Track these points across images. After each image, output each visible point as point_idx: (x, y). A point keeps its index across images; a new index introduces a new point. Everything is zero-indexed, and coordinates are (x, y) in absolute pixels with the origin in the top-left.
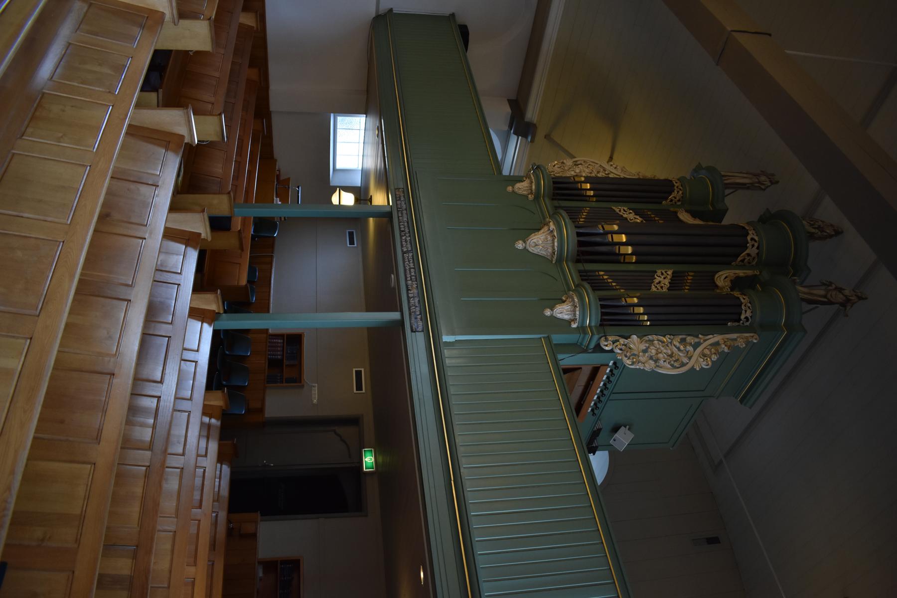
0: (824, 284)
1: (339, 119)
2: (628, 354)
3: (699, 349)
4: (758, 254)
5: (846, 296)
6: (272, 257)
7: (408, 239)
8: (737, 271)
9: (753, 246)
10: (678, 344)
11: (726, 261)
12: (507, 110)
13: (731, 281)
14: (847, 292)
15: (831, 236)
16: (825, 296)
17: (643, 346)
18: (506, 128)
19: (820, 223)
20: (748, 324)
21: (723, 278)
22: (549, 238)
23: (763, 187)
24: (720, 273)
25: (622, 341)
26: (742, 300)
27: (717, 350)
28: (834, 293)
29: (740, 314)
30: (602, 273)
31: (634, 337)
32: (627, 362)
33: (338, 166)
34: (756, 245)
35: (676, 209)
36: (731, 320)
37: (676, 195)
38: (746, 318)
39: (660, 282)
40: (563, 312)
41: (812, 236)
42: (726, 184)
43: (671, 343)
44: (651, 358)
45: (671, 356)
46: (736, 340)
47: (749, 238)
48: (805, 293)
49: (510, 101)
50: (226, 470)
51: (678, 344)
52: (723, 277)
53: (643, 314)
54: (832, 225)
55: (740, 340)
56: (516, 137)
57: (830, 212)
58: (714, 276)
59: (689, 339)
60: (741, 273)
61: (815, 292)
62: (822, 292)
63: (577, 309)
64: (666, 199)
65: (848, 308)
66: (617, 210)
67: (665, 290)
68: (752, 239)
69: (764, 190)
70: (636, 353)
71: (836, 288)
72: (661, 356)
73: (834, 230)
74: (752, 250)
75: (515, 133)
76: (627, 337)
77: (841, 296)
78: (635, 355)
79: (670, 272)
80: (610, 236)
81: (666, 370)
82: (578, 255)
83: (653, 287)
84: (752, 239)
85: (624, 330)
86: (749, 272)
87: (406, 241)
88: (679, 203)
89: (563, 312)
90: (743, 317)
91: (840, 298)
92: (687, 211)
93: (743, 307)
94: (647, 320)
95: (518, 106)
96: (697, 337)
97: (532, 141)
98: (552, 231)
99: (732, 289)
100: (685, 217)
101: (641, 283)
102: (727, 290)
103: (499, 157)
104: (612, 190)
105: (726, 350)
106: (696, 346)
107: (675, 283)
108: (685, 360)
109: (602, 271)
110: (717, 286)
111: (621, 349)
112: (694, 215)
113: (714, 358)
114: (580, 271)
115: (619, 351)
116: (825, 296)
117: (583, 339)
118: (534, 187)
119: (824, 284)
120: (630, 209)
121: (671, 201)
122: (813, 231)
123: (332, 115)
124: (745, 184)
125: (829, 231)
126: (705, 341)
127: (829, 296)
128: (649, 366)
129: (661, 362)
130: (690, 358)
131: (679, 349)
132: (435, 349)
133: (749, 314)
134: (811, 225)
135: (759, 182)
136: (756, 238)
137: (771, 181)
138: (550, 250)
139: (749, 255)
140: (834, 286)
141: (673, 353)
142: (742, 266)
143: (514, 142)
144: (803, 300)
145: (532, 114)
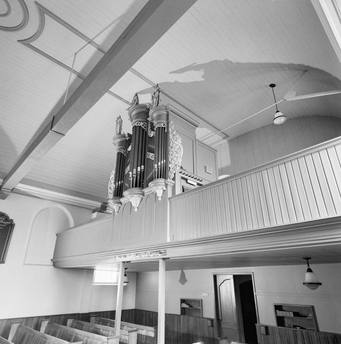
0: (153, 99)
4: (143, 122)
5: (157, 91)
6: (146, 311)
9: (140, 124)
14: (155, 91)
15: (137, 97)
16: (157, 98)
21: (152, 134)
23: (121, 121)
28: (155, 95)
29: (162, 127)
30: (147, 178)
33: (116, 282)
34: (139, 123)
39: (151, 157)
47: (137, 125)
48: (155, 105)
65: (160, 90)
71: (154, 94)
75: (105, 211)
80: (159, 167)
84: (137, 124)
88: (125, 150)
91: (157, 93)
108: (178, 147)
116: (157, 98)
122: (135, 103)
124: (120, 127)
126: (171, 140)
127: (156, 97)
134: (134, 104)
135: (120, 122)
136: (137, 123)
140: (154, 95)
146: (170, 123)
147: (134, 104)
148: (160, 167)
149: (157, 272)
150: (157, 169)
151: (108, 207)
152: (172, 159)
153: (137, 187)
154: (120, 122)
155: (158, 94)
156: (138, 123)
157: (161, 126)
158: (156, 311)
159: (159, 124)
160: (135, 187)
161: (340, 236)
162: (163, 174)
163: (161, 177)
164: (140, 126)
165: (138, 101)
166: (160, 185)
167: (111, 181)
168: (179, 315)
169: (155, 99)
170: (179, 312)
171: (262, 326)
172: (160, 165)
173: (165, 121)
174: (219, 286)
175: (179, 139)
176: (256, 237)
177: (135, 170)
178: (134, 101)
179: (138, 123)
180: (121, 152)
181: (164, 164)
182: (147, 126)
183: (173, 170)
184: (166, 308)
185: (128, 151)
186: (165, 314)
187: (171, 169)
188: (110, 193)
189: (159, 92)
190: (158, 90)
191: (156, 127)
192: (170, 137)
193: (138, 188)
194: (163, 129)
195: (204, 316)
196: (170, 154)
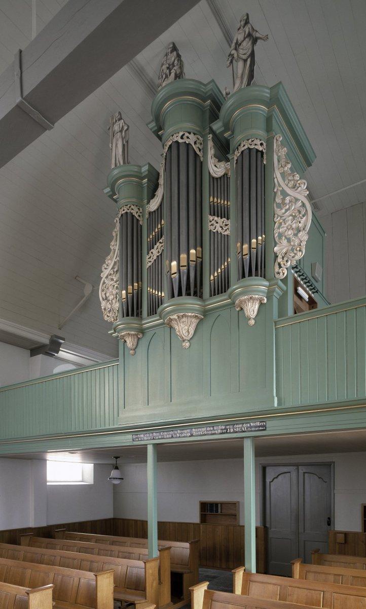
0: (231, 62)
1: (48, 478)
2: (292, 255)
3: (289, 191)
4: (195, 134)
5: (245, 39)
6: (136, 521)
7: (179, 431)
8: (209, 156)
9: (188, 138)
10: (283, 211)
11: (199, 165)
12: (40, 357)
13: (220, 161)
14: (240, 37)
15: (179, 56)
16: (245, 61)
17: (284, 242)
18: (52, 359)
19: (164, 67)
20: (265, 144)
21: (216, 169)
22: (184, 319)
23: (125, 128)
24: (211, 171)
25: (279, 260)
26: (246, 147)
27: (289, 175)
28: (241, 51)
29: (257, 151)
30: (212, 278)
31: (276, 249)
32: (299, 256)
33: (81, 479)
34: (187, 134)
35: (147, 212)
36: (262, 161)
37: (135, 211)
38: (262, 144)
39: (221, 227)
40: (252, 309)
41: (178, 76)
42: (124, 163)
43: (281, 217)
44: (296, 235)
45: (294, 217)
46: (279, 157)
47: (180, 141)
48: (242, 82)
49: (32, 355)
50: (330, 557)
51: (283, 211)
52: (215, 169)
53: (257, 239)
54: (166, 55)
55: (280, 151)
56: (60, 352)
57: (151, 56)
58: (213, 178)
59: (278, 200)
60: (211, 152)
61: (240, 72)
62: (241, 64)
63: (254, 296)
64: (138, 220)
65: (258, 35)
66: (150, 264)
67: (229, 222)
68: (182, 138)
69: (128, 126)
70: (290, 248)
71: (236, 49)
72: (294, 226)
73: (172, 52)
74: (192, 139)
75: (57, 352)
76: (276, 257)
77: (244, 43)
78: (292, 250)
79: (211, 218)
80: (181, 268)
81: (307, 221)
82: (196, 296)
83: (226, 233)
84: (182, 138)
85: (270, 258)
86: (210, 144)
87: (182, 433)
88: (141, 209)
89: (252, 309)
90: (260, 148)
91: (247, 44)
92: (148, 202)
93: (252, 147)
94: (262, 236)
95: (36, 350)
96: (275, 193)
97: (63, 339)
98: (178, 317)
99: (227, 160)
100: (154, 205)
101: (222, 244)
102: (228, 165)
103: (72, 367)
104: (132, 266)
105: (289, 166)
106: (284, 194)
107: (223, 213)
108: (299, 204)
109: (211, 277)
110: (225, 175)
111: (287, 261)
112: (152, 196)
113: (297, 177)
114: (148, 316)
115: (289, 263)
116: (245, 61)
117: (277, 293)
118: (133, 333)
119: (231, 62)
120: (148, 254)
121: (139, 216)
122: (173, 75)
123: (48, 484)
124: (124, 145)
125: (173, 57)
126: (279, 185)
127: (244, 57)
128: (304, 236)
129: (300, 225)
130: (297, 200)
131: (286, 211)
132: (284, 413)
133: (259, 142)
134: (167, 77)
135: (121, 131)
136: (181, 134)
137: (120, 119)
138: (193, 320)
139: (195, 143)
140: (234, 52)
141: (291, 215)
142: (204, 150)
143: (63, 354)
144: (249, 84)
145: (45, 340)
146: (275, 141)
147: (167, 77)
148: (184, 269)
149: (143, 464)
150: (249, 255)
151: (62, 346)
152: (280, 235)
153: (182, 295)
154: (121, 131)
155: (251, 47)
156: (184, 135)
157: (256, 147)
158: (143, 518)
159: (250, 141)
160: (178, 296)
161: (365, 425)
162: (257, 267)
163: (250, 274)
164: (189, 145)
165: (181, 67)
166: (254, 291)
167: (104, 283)
168: (197, 524)
169: (240, 64)
170: (196, 519)
171: (340, 533)
172: (186, 264)
173: (262, 133)
174: (270, 482)
175: (302, 186)
176: (319, 415)
177: (183, 256)
178: (168, 68)
179: (184, 135)
180: (132, 211)
181: (257, 248)
182: (202, 146)
183: (285, 259)
184: (159, 515)
185: (150, 213)
186: (158, 522)
187: (280, 256)
188: (105, 309)
189: (255, 41)
190: (250, 35)
191: (242, 149)
192: (276, 180)
193: (192, 297)
194: (259, 154)
195: (241, 524)
196: (275, 223)
